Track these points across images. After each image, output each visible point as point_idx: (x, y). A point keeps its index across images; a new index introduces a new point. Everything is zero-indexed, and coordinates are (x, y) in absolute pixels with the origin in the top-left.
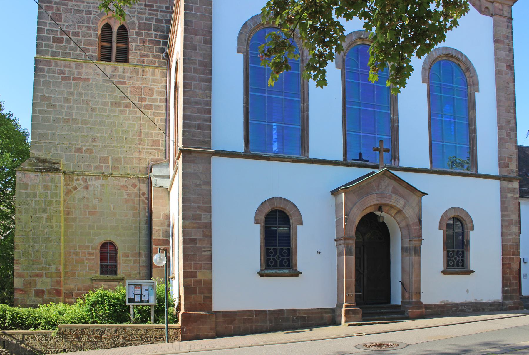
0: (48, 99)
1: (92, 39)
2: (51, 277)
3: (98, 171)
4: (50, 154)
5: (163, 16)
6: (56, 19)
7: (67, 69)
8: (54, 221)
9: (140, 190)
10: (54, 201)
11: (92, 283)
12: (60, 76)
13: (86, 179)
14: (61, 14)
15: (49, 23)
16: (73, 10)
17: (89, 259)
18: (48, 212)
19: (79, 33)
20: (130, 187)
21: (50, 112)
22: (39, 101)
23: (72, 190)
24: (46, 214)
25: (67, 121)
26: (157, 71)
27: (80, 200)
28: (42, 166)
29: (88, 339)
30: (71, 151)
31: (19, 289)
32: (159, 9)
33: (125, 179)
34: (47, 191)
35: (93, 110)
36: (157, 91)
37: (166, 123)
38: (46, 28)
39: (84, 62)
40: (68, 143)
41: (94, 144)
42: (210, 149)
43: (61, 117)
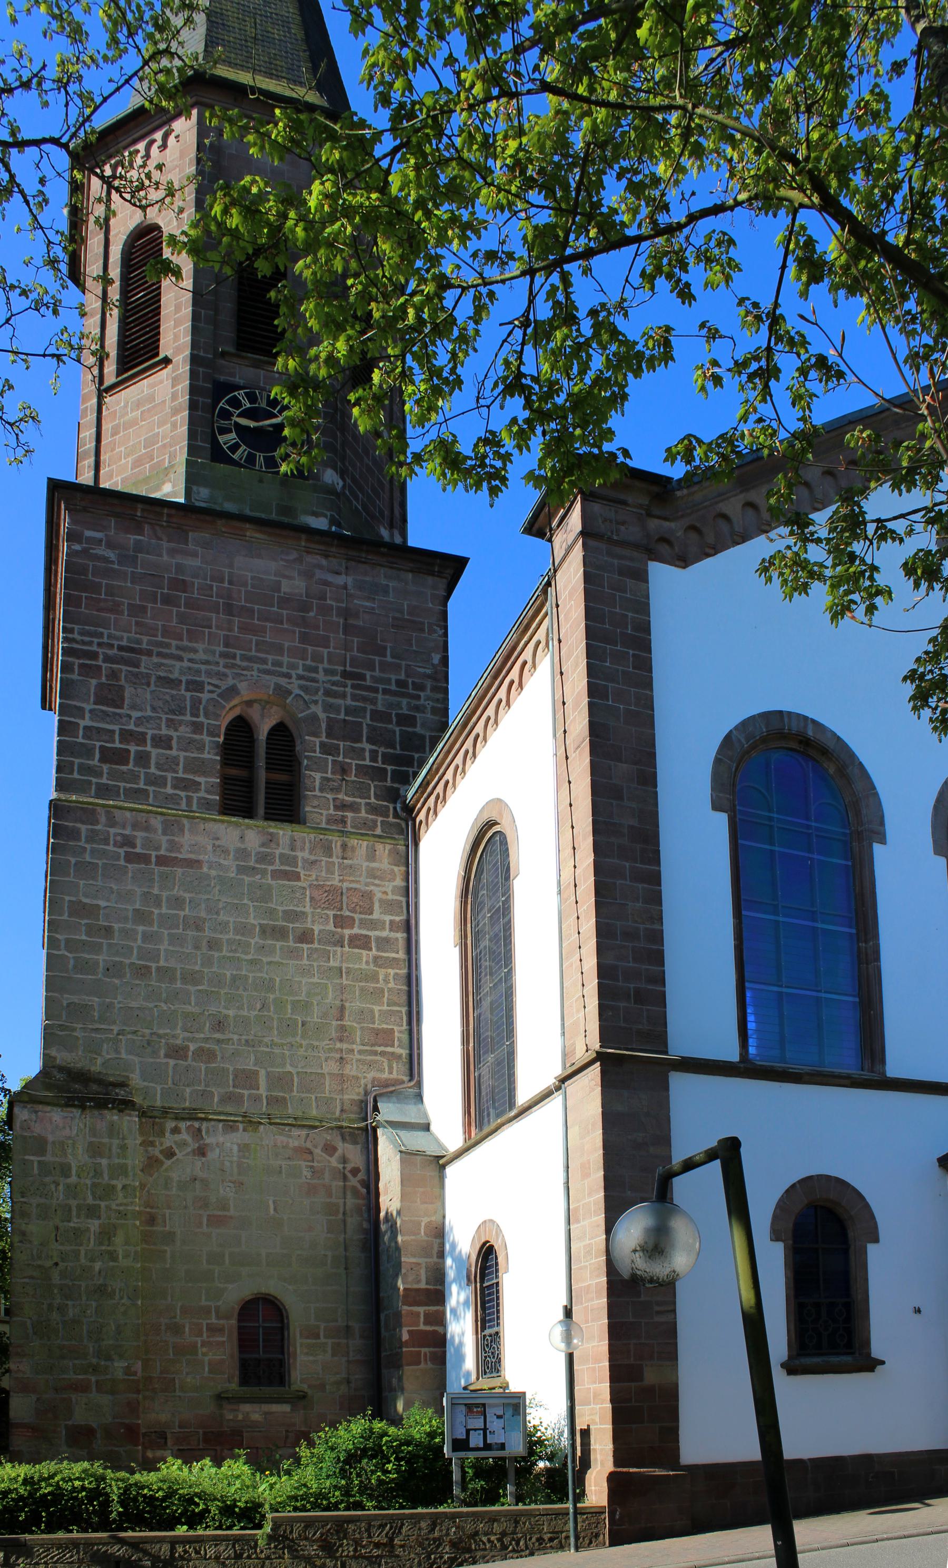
0: (92, 911)
1: (206, 756)
3: (229, 1109)
6: (110, 696)
7: (140, 834)
8: (119, 1239)
9: (344, 1160)
10: (120, 1187)
12: (122, 851)
13: (199, 1130)
14: (122, 688)
15: (91, 711)
19: (170, 738)
20: (318, 1151)
21: (96, 948)
22: (65, 917)
23: (161, 1157)
24: (97, 1222)
25: (142, 972)
26: (379, 847)
29: (355, 1550)
30: (155, 1053)
32: (381, 687)
33: (304, 1132)
34: (98, 1160)
35: (213, 944)
36: (380, 901)
37: (409, 984)
38: (82, 723)
39: (187, 817)
41: (217, 1036)
42: (666, 1053)
43: (127, 961)
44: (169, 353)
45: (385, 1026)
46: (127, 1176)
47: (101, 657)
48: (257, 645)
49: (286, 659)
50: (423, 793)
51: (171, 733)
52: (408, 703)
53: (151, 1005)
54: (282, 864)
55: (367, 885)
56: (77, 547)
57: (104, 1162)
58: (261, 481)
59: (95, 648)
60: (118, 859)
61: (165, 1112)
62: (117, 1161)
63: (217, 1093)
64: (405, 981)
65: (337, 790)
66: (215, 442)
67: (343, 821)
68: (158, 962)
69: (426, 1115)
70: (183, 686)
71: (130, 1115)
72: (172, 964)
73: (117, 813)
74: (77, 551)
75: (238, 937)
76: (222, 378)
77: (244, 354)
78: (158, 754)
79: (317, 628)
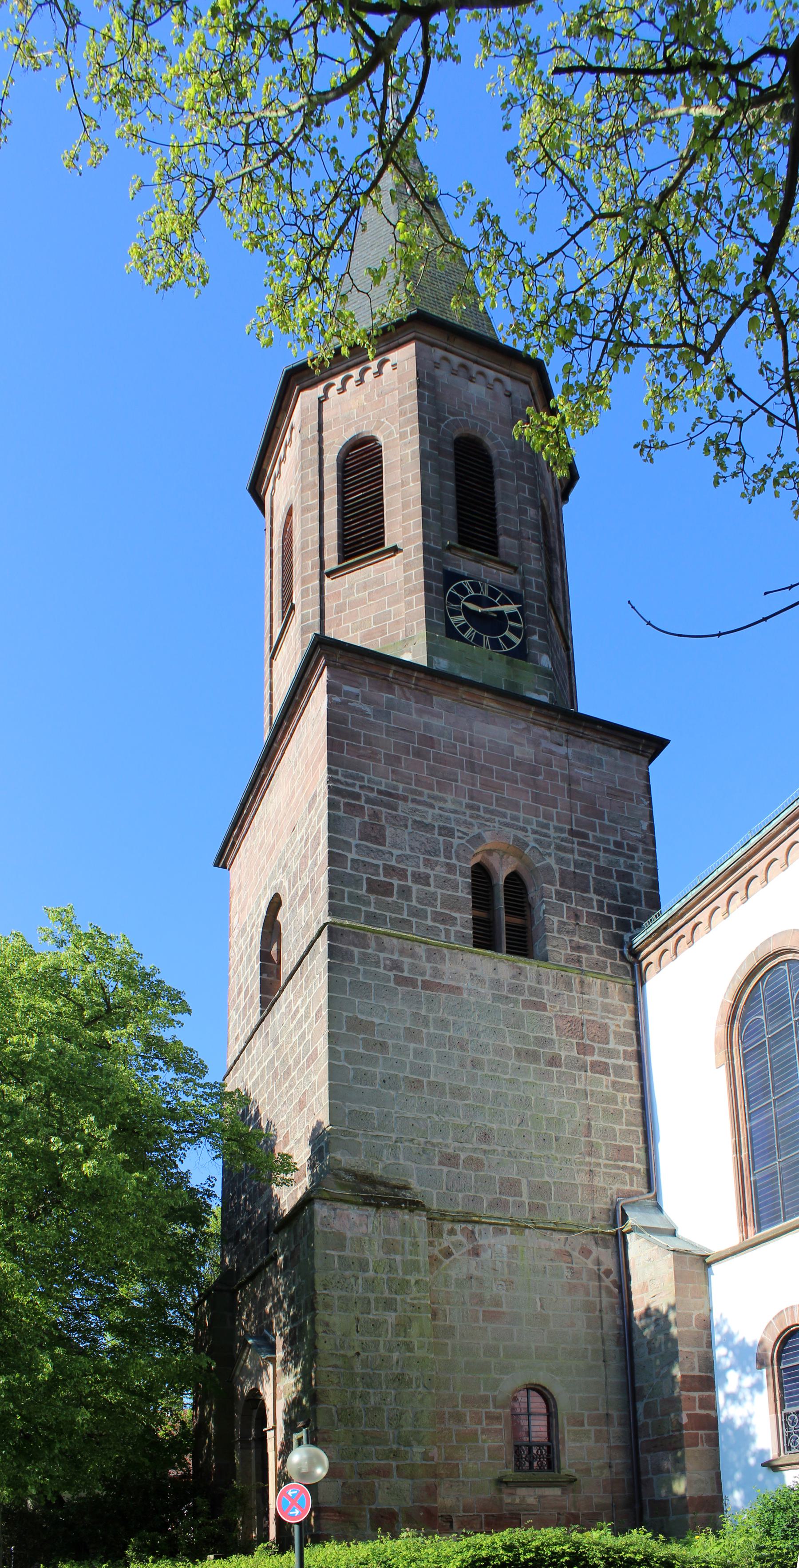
0: (368, 1027)
1: (460, 894)
2: (412, 1477)
4: (381, 1165)
5: (611, 863)
6: (373, 834)
7: (407, 960)
8: (414, 1331)
9: (598, 1263)
10: (413, 1282)
11: (500, 1491)
13: (473, 1232)
15: (357, 846)
16: (410, 823)
17: (489, 1431)
18: (399, 1308)
19: (428, 877)
20: (576, 1254)
21: (373, 1061)
22: (344, 1031)
23: (441, 1257)
24: (393, 1315)
25: (415, 1085)
26: (611, 985)
27: (460, 1283)
28: (366, 1192)
30: (430, 1160)
31: (331, 1510)
32: (602, 846)
33: (563, 1236)
34: (393, 1256)
36: (615, 1032)
40: (422, 1140)
41: (484, 1146)
43: (401, 1075)
44: (399, 544)
45: (625, 1143)
46: (419, 1272)
47: (363, 798)
48: (497, 800)
49: (521, 815)
50: (656, 938)
51: (429, 871)
52: (625, 862)
53: (425, 1116)
54: (531, 995)
55: (602, 1018)
56: (337, 699)
57: (398, 1258)
58: (490, 659)
59: (357, 790)
60: (389, 981)
61: (443, 1215)
62: (410, 1257)
63: (486, 1198)
64: (639, 1104)
65: (572, 933)
66: (448, 622)
67: (579, 961)
68: (429, 1077)
69: (669, 1222)
70: (436, 831)
71: (420, 1215)
72: (440, 1079)
73: (386, 939)
74: (337, 703)
75: (497, 1058)
76: (449, 568)
77: (468, 549)
78: (418, 889)
79: (546, 790)
